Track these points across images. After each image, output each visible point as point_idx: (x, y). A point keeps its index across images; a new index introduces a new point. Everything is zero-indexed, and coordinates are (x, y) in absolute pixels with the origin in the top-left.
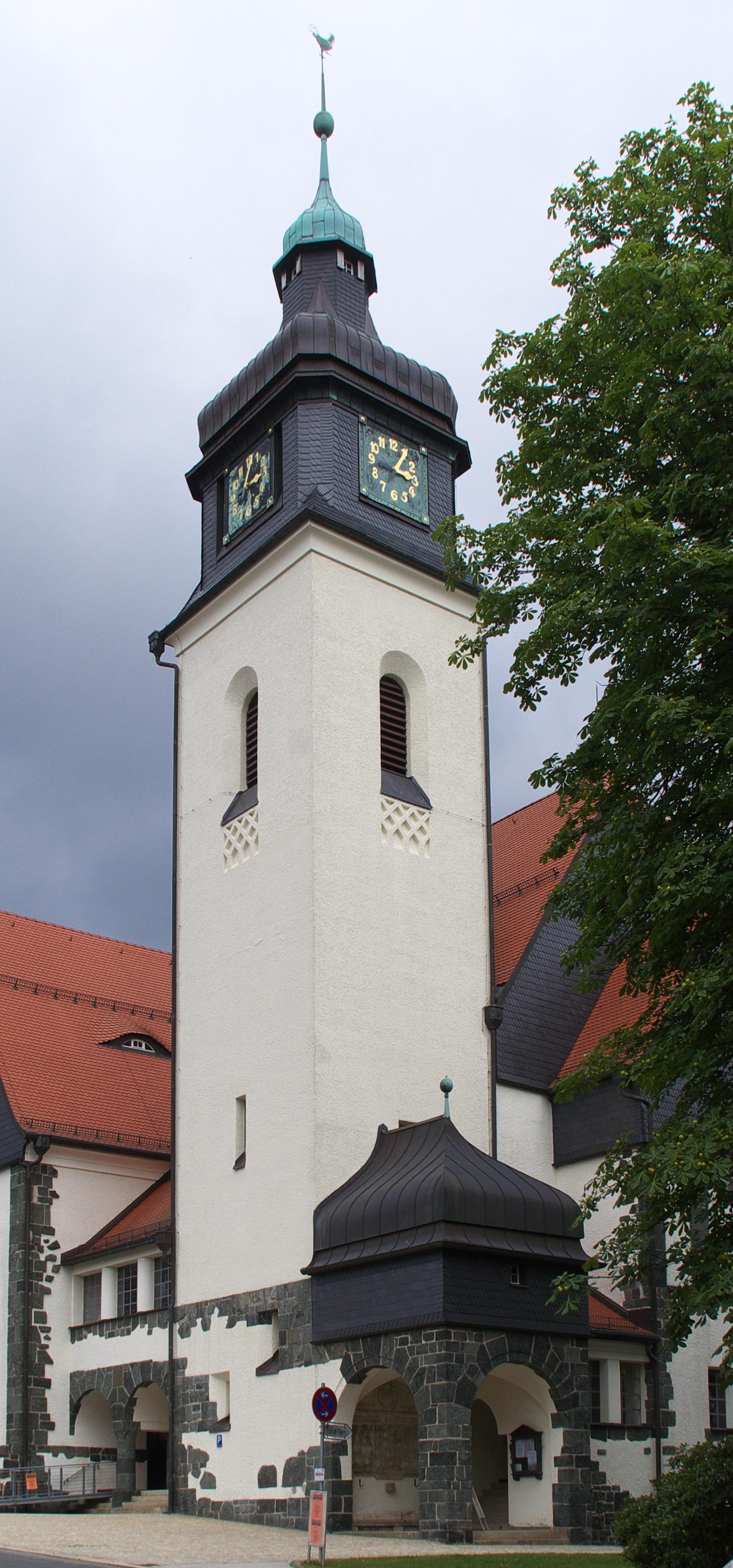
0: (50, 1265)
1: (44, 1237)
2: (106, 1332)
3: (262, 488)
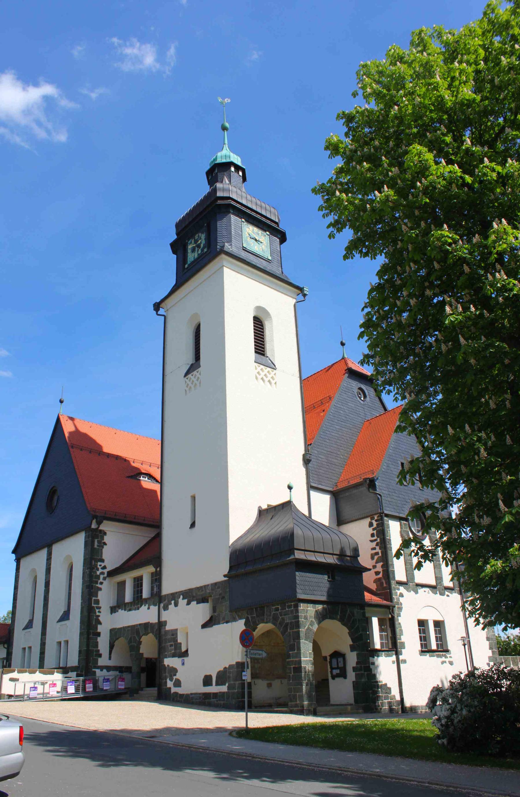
0: (102, 577)
1: (99, 563)
2: (128, 609)
3: (202, 245)
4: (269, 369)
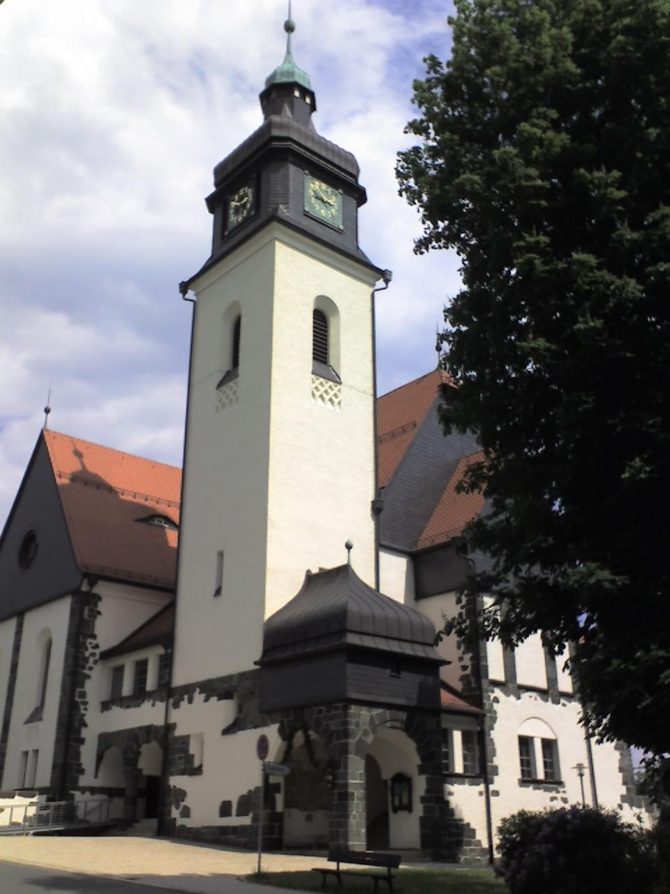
1: (89, 640)
2: (446, 314)
3: (248, 206)
4: (331, 383)
